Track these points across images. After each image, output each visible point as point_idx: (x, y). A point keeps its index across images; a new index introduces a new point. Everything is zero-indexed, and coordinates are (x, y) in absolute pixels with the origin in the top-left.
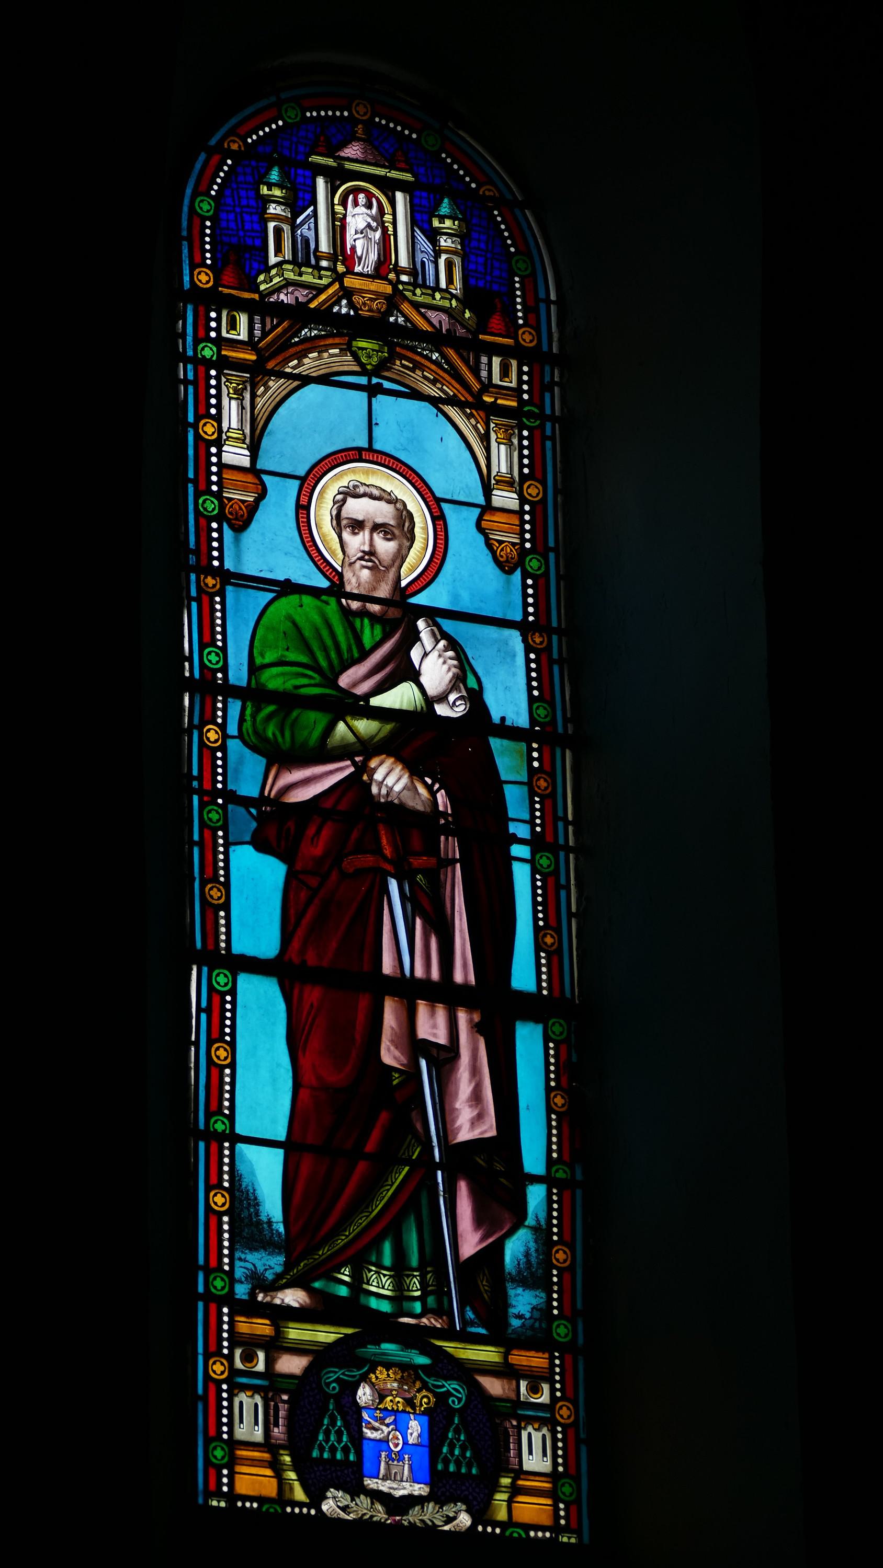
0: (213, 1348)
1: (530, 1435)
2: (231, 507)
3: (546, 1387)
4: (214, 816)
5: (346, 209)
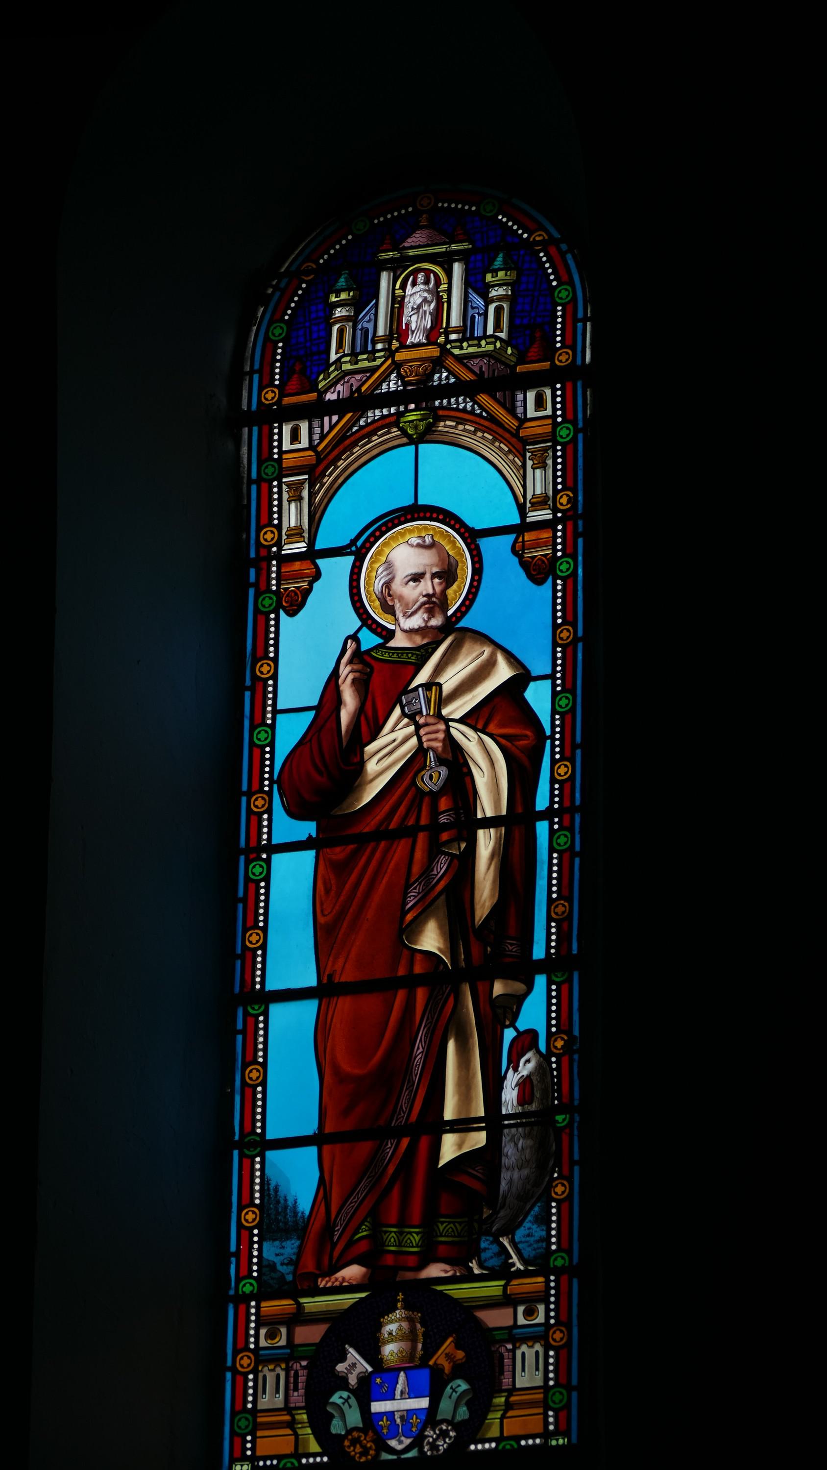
0: (241, 1345)
1: (523, 1354)
2: (288, 595)
3: (541, 1308)
4: (254, 1075)
5: (404, 291)
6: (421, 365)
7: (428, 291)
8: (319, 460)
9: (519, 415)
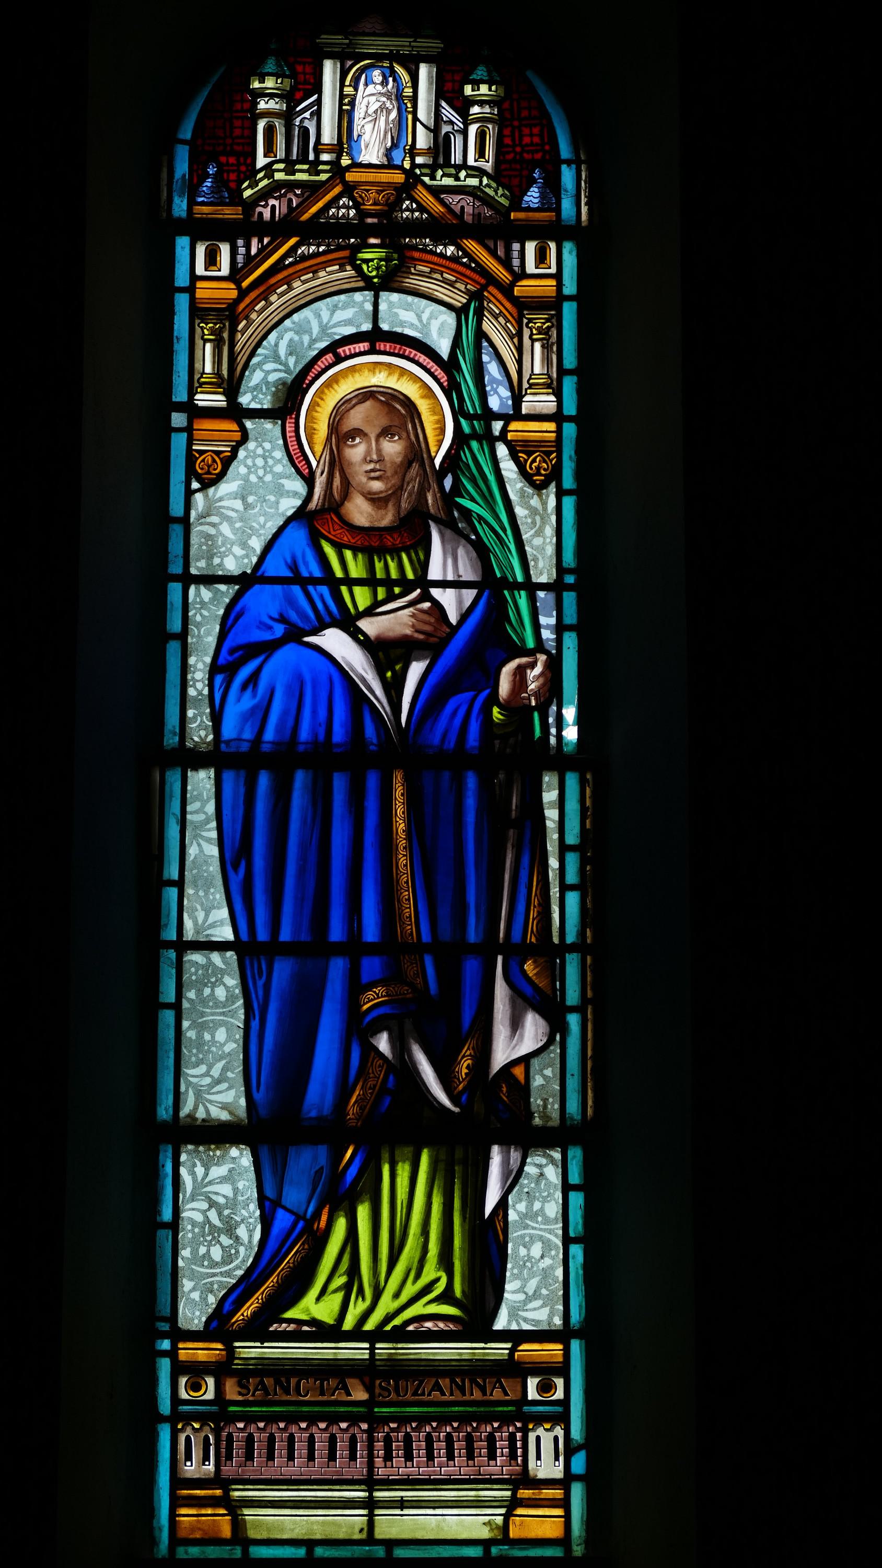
1: (538, 1439)
2: (203, 460)
3: (559, 1382)
5: (356, 89)
6: (382, 191)
7: (388, 95)
8: (243, 293)
9: (516, 269)
